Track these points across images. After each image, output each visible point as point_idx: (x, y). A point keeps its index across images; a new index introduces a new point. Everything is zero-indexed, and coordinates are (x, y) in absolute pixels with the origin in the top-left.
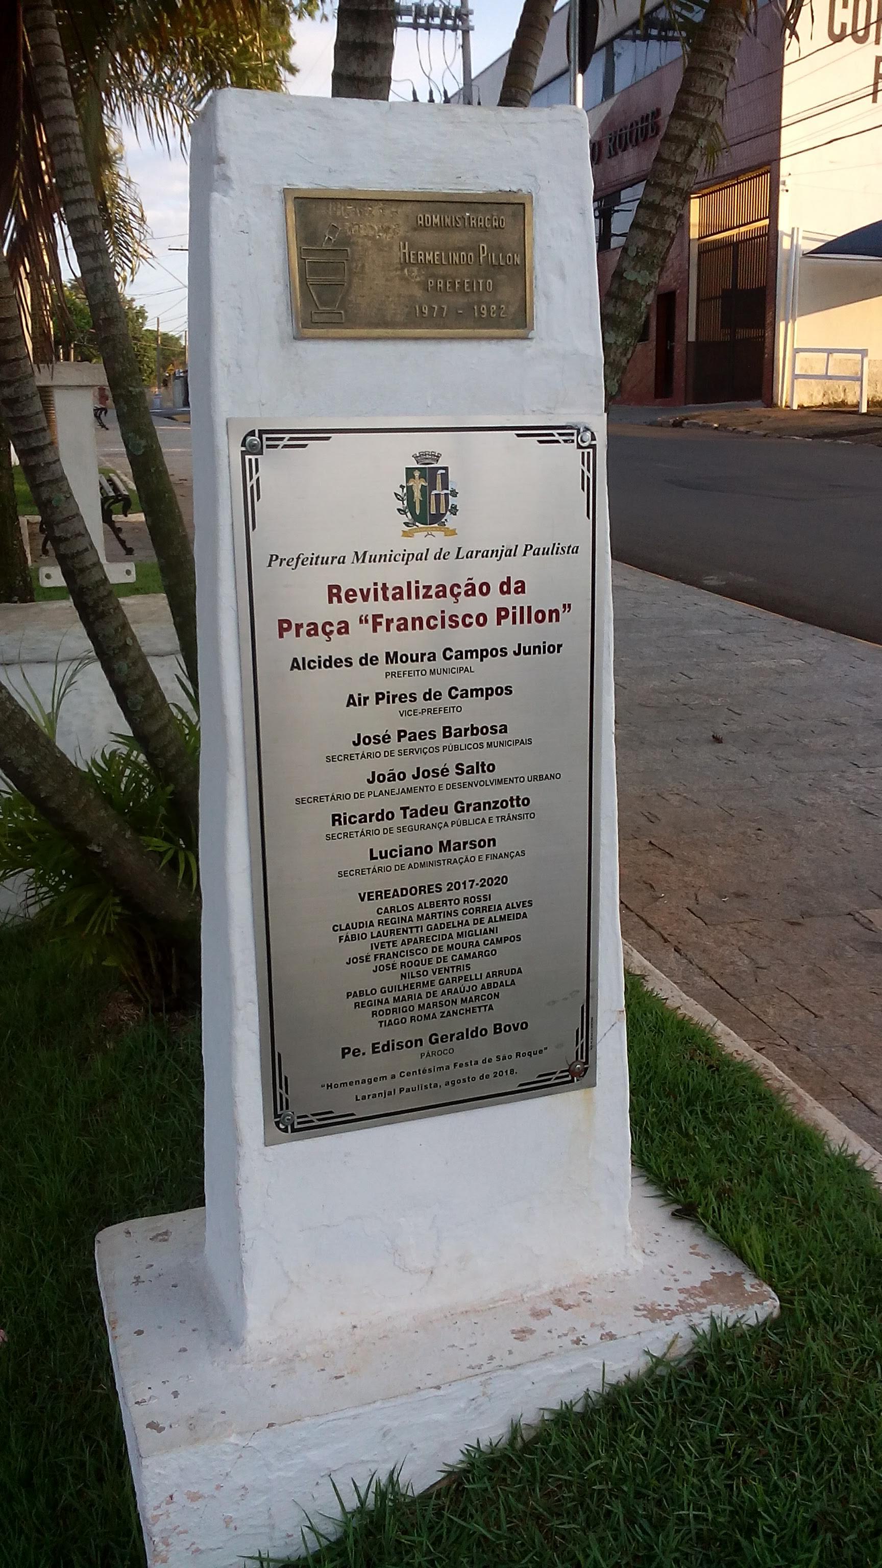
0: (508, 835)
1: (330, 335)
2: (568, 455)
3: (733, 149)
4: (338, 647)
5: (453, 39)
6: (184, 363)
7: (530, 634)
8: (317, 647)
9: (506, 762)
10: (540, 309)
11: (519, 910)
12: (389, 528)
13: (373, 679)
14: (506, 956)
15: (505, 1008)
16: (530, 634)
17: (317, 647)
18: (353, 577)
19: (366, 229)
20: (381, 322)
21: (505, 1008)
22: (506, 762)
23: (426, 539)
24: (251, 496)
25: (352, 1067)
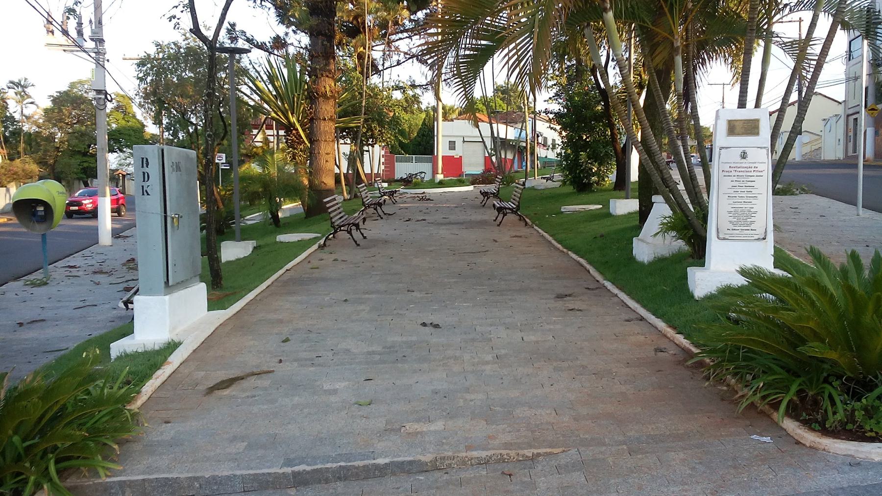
0: (754, 201)
1: (824, 35)
2: (765, 151)
3: (805, 126)
4: (730, 174)
5: (430, 165)
6: (711, 141)
7: (759, 174)
8: (727, 174)
9: (754, 191)
10: (761, 133)
11: (755, 212)
12: (739, 159)
13: (735, 179)
14: (753, 219)
15: (753, 227)
16: (759, 174)
17: (727, 174)
18: (732, 165)
19: (737, 124)
20: (738, 134)
21: (753, 227)
22: (754, 191)
23: (743, 161)
24: (720, 155)
25: (729, 232)
